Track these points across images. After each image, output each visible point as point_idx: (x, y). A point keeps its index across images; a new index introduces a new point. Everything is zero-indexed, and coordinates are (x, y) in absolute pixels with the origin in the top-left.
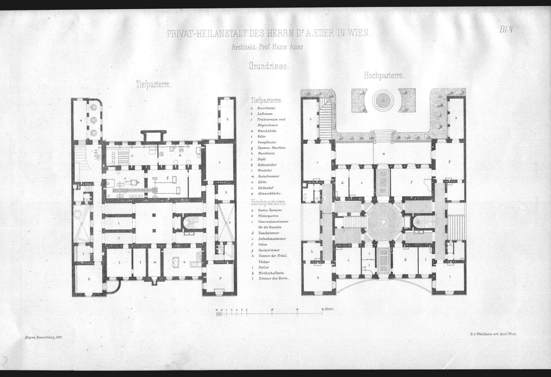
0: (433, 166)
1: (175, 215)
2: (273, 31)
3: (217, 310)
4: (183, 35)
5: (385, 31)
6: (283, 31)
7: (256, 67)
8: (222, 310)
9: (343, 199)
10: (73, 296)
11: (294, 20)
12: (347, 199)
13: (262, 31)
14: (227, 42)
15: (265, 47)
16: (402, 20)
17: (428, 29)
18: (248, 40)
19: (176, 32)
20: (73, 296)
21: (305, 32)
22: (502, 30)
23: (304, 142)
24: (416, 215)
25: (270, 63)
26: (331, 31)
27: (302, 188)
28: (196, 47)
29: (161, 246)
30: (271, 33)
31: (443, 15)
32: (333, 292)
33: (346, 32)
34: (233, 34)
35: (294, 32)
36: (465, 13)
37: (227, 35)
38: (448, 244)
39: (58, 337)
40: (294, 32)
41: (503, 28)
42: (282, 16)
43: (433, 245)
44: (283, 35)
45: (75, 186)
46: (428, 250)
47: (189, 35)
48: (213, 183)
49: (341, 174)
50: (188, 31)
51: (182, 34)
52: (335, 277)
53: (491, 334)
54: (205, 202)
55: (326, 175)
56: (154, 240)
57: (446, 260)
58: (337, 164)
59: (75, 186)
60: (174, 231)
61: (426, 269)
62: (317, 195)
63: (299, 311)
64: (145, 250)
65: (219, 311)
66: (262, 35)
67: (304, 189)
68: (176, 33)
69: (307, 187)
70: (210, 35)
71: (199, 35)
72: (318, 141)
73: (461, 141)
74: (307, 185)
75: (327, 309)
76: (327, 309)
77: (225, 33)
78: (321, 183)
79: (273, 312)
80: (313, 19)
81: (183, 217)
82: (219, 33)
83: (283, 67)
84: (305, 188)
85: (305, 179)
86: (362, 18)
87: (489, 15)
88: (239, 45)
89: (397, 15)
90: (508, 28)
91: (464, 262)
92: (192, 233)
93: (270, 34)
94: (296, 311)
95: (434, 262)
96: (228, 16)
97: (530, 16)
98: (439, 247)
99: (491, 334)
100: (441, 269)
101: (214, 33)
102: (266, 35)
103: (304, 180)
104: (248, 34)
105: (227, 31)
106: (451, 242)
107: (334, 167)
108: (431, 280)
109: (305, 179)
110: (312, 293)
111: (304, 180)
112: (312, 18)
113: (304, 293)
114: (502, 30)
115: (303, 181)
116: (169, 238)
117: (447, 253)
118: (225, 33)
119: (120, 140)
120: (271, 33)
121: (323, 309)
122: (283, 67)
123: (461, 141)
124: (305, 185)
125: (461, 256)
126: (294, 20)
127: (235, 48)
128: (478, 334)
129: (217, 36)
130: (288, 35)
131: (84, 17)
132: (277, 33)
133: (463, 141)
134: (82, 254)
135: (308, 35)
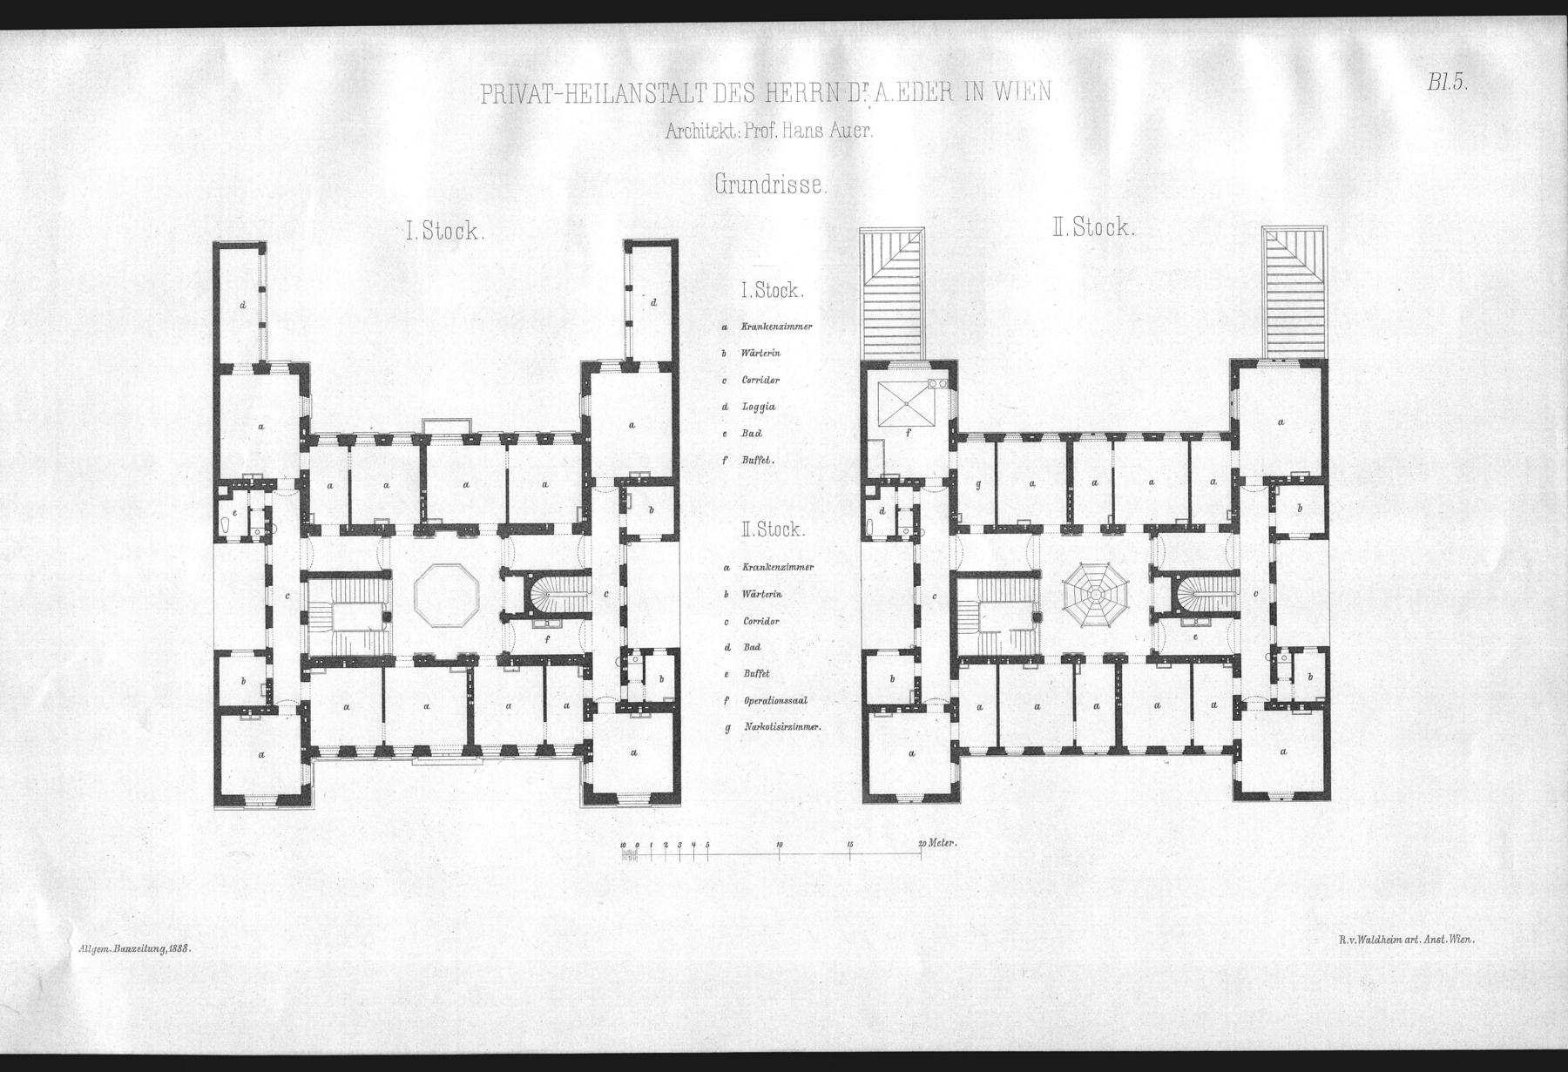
0: (1232, 436)
1: (505, 573)
2: (780, 87)
4: (526, 100)
6: (809, 87)
8: (637, 845)
9: (977, 529)
10: (309, 804)
11: (838, 58)
12: (988, 530)
13: (749, 87)
16: (1141, 54)
17: (1219, 77)
18: (707, 112)
20: (309, 804)
21: (873, 89)
22: (1435, 85)
23: (221, 369)
24: (1186, 574)
28: (560, 129)
29: (1117, 660)
30: (769, 91)
31: (1259, 43)
32: (303, 798)
33: (990, 92)
34: (668, 93)
35: (837, 90)
37: (651, 98)
38: (630, 659)
39: (174, 948)
40: (837, 90)
41: (1436, 77)
42: (803, 45)
43: (585, 662)
45: (223, 491)
46: (573, 671)
47: (543, 98)
48: (612, 482)
49: (326, 462)
51: (519, 93)
52: (958, 752)
53: (1399, 940)
54: (1237, 531)
55: (283, 462)
57: (1274, 701)
58: (962, 429)
60: (505, 617)
61: (1216, 729)
62: (258, 520)
63: (712, 850)
64: (1188, 666)
65: (630, 846)
66: (749, 97)
67: (221, 503)
68: (507, 92)
69: (877, 497)
70: (602, 99)
72: (262, 368)
73: (664, 367)
74: (878, 491)
75: (933, 842)
77: (644, 92)
78: (269, 485)
79: (783, 849)
80: (890, 54)
81: (531, 578)
84: (223, 498)
85: (225, 474)
86: (1028, 52)
90: (1451, 77)
91: (1324, 706)
92: (1205, 621)
93: (772, 95)
95: (590, 708)
96: (650, 46)
97: (1517, 45)
98: (605, 666)
99: (1399, 940)
100: (1256, 728)
101: (612, 92)
103: (224, 476)
104: (709, 95)
105: (651, 87)
106: (1285, 652)
107: (309, 441)
108: (1230, 758)
109: (225, 474)
110: (891, 799)
111: (224, 476)
113: (869, 798)
114: (1435, 85)
117: (1274, 679)
118: (644, 92)
120: (769, 91)
121: (922, 844)
123: (664, 367)
124: (870, 490)
125: (1315, 692)
126: (838, 58)
128: (1362, 939)
129: (622, 99)
130: (825, 97)
132: (792, 91)
133: (671, 367)
134: (242, 686)
135: (881, 98)
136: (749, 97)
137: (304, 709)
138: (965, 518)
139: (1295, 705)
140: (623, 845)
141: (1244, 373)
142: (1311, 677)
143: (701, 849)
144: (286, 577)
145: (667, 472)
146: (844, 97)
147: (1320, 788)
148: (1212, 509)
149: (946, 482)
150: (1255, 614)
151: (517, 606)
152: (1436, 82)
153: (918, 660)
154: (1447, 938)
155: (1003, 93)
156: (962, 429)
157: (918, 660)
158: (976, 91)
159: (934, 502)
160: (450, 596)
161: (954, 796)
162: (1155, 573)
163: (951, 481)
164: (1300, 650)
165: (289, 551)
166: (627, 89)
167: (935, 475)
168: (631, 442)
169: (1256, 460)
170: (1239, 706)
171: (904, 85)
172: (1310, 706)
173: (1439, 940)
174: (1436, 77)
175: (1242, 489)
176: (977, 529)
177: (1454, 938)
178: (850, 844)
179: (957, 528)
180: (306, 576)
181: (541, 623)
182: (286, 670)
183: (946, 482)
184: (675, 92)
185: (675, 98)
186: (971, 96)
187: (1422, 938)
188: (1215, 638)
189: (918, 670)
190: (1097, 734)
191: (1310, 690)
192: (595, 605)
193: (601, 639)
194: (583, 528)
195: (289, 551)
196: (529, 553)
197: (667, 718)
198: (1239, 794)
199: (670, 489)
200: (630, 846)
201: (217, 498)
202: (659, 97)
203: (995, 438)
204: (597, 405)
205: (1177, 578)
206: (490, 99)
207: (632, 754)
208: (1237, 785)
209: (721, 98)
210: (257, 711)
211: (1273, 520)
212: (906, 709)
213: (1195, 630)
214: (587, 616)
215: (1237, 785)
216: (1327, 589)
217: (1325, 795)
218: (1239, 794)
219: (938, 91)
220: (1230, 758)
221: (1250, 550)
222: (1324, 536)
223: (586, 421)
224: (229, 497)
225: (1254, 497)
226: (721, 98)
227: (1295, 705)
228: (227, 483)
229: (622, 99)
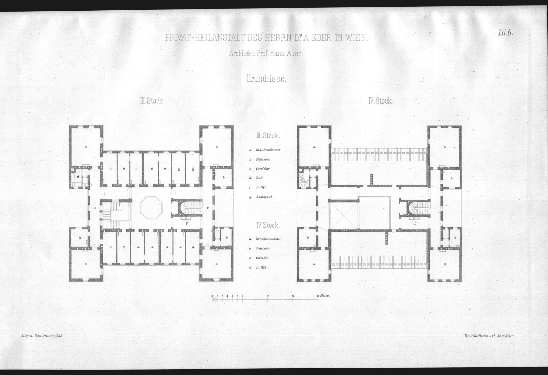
0: (200, 152)
1: (172, 200)
3: (213, 296)
5: (381, 28)
7: (253, 80)
9: (110, 185)
13: (260, 35)
14: (225, 46)
15: (263, 53)
16: (399, 19)
18: (246, 45)
19: (175, 35)
24: (184, 201)
25: (268, 75)
26: (329, 36)
27: (298, 172)
29: (159, 232)
30: (268, 37)
31: (439, 15)
33: (344, 37)
35: (293, 36)
36: (462, 13)
37: (225, 39)
38: (216, 230)
40: (293, 36)
41: (501, 31)
42: (280, 16)
44: (281, 39)
45: (72, 170)
47: (187, 39)
49: (109, 159)
50: (186, 35)
51: (180, 38)
53: (487, 336)
56: (150, 190)
58: (105, 149)
59: (72, 170)
63: (244, 298)
66: (260, 39)
69: (303, 172)
70: (208, 39)
71: (197, 39)
75: (322, 295)
76: (322, 295)
77: (223, 37)
79: (269, 298)
81: (181, 202)
82: (217, 38)
83: (281, 79)
86: (358, 19)
87: (485, 15)
88: (236, 50)
89: (395, 15)
91: (460, 248)
94: (291, 298)
96: (227, 16)
99: (487, 336)
101: (212, 37)
102: (264, 39)
104: (246, 38)
105: (225, 36)
106: (446, 229)
112: (308, 18)
115: (299, 167)
116: (166, 223)
117: (442, 239)
118: (223, 37)
119: (118, 150)
120: (268, 37)
121: (318, 296)
122: (281, 79)
125: (456, 243)
126: (292, 23)
127: (233, 53)
128: (473, 336)
129: (215, 39)
130: (286, 39)
131: (84, 18)
132: (275, 37)
135: (306, 40)
136: (260, 39)
137: (100, 248)
138: (147, 181)
139: (221, 248)
140: (213, 296)
141: (204, 130)
142: (227, 237)
143: (240, 297)
144: (95, 201)
145: (229, 165)
146: (293, 38)
147: (230, 277)
148: (193, 179)
149: (99, 168)
150: (435, 216)
151: (405, 213)
152: (502, 32)
153: (89, 231)
154: (505, 336)
155: (349, 38)
156: (105, 149)
157: (89, 231)
158: (339, 37)
159: (95, 174)
160: (153, 208)
161: (101, 279)
162: (401, 201)
163: (100, 168)
164: (452, 228)
165: (96, 192)
166: (217, 36)
167: (95, 164)
168: (445, 155)
169: (209, 161)
170: (202, 248)
171: (324, 35)
172: (227, 248)
173: (503, 336)
174: (501, 31)
175: (203, 171)
176: (110, 185)
177: (507, 336)
178: (293, 296)
179: (102, 185)
180: (102, 201)
181: (411, 218)
182: (95, 232)
183: (99, 168)
184: (235, 37)
185: (306, 40)
186: (338, 39)
187: (496, 335)
188: (194, 223)
189: (317, 234)
190: (153, 258)
191: (227, 242)
192: (204, 212)
193: (206, 224)
194: (200, 185)
195: (96, 192)
196: (180, 193)
197: (458, 251)
198: (201, 279)
199: (230, 170)
200: (215, 296)
201: (70, 172)
202: (228, 39)
203: (117, 152)
204: (205, 140)
205: (409, 202)
206: (169, 39)
207: (217, 264)
208: (201, 276)
209: (250, 39)
210: (314, 248)
211: (214, 182)
212: (314, 248)
213: (414, 221)
214: (201, 216)
215: (201, 276)
216: (464, 207)
217: (231, 280)
218: (201, 279)
219: (326, 37)
220: (198, 266)
221: (206, 192)
222: (232, 188)
223: (201, 145)
224: (74, 172)
225: (207, 174)
226: (250, 39)
227: (221, 248)
228: (301, 168)
229: (215, 39)
